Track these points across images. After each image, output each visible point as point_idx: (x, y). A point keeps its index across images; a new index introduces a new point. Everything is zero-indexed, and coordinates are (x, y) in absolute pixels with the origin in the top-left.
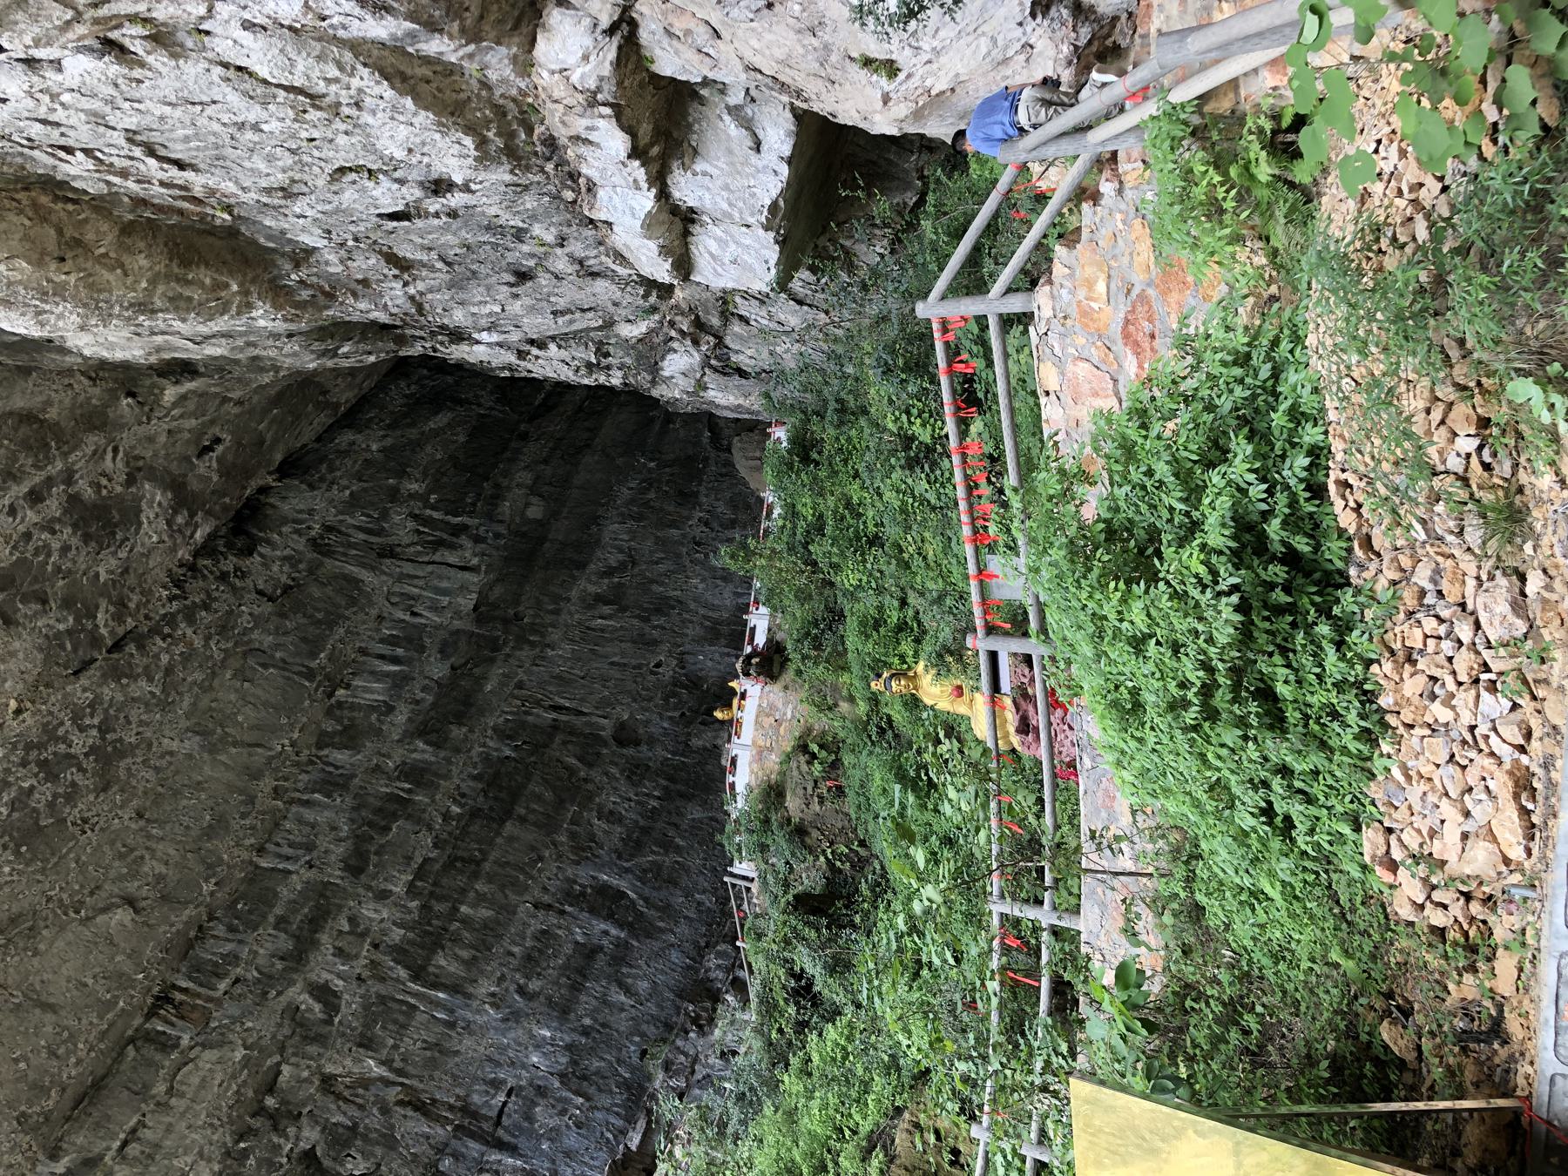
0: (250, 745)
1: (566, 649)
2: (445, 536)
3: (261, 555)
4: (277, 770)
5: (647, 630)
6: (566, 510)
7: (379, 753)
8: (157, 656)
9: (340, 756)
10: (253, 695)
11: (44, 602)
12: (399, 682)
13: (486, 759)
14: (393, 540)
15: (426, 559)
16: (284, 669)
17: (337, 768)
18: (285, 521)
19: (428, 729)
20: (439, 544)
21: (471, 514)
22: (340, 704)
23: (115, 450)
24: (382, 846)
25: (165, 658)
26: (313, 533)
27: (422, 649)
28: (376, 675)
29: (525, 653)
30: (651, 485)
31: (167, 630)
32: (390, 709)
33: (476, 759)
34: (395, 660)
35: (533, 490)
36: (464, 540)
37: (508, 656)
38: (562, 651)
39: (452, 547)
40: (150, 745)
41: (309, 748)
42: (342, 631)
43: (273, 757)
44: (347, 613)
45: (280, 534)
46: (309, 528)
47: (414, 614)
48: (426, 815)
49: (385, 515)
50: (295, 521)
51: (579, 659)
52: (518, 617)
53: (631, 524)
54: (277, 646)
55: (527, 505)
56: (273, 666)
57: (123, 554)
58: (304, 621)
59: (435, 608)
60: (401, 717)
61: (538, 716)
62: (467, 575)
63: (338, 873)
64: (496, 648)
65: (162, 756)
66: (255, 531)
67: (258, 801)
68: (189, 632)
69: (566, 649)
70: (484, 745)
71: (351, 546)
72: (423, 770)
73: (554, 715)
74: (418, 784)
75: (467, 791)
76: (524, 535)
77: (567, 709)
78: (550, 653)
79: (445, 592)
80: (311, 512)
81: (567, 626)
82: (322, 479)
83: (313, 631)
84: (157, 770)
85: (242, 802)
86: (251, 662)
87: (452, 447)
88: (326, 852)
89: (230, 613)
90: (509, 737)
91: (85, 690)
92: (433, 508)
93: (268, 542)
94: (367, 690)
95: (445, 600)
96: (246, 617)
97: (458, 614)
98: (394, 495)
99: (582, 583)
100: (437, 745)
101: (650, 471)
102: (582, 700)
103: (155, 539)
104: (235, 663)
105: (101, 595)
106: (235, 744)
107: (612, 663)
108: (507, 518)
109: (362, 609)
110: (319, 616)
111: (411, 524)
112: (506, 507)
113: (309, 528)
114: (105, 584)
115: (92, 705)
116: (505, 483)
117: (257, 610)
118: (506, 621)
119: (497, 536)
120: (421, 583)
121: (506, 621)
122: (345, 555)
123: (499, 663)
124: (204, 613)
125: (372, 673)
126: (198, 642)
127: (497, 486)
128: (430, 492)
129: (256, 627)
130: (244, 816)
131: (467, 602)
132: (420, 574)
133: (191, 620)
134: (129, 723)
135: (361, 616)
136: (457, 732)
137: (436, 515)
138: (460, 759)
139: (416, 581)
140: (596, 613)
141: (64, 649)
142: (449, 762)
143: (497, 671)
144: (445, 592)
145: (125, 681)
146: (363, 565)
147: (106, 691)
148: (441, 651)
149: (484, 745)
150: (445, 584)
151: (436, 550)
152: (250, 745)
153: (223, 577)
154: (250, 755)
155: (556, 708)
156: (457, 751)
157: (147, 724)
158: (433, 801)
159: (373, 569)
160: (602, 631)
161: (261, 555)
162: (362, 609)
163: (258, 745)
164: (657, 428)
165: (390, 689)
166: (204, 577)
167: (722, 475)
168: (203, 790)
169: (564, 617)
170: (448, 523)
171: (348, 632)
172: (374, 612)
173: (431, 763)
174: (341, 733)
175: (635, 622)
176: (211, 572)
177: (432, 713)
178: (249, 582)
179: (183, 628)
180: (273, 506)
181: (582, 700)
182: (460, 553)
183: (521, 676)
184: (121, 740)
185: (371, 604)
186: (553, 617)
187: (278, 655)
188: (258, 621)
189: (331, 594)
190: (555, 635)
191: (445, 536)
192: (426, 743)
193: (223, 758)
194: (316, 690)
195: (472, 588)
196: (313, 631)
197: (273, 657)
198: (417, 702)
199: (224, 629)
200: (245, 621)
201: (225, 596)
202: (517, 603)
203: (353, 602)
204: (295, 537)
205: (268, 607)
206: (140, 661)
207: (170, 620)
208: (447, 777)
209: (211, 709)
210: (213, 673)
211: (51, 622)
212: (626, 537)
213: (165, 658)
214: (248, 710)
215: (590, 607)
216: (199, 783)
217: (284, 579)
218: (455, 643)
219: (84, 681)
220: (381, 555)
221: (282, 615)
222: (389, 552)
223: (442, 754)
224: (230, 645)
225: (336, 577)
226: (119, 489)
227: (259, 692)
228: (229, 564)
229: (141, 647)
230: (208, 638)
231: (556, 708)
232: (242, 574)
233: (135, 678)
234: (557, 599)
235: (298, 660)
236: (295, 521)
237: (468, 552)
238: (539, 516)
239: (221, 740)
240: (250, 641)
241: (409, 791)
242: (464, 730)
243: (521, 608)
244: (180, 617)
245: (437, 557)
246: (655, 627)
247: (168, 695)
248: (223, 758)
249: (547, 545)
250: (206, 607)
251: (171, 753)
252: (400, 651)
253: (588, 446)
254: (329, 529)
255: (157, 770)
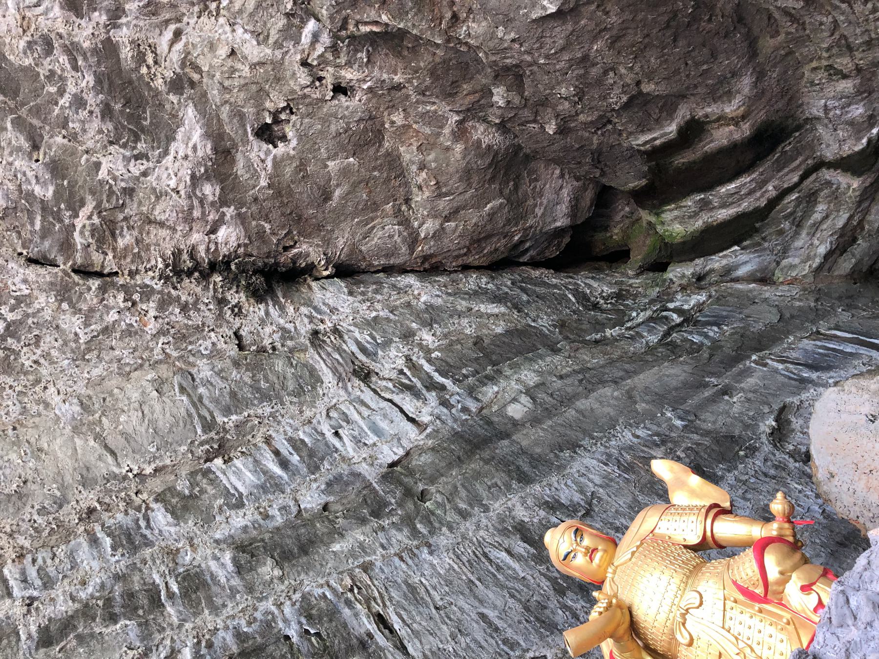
0: (106, 447)
1: (444, 562)
2: (419, 385)
3: (267, 313)
4: (108, 492)
5: (553, 604)
6: (550, 423)
7: (191, 540)
8: (108, 308)
9: (161, 517)
10: (151, 407)
11: (36, 147)
12: (271, 485)
13: (268, 625)
14: (373, 366)
15: (388, 396)
16: (194, 404)
17: (148, 526)
18: (309, 303)
19: (247, 551)
20: (410, 388)
21: (456, 381)
22: (207, 473)
23: (178, 34)
24: (92, 635)
25: (113, 316)
26: (321, 327)
27: (314, 469)
28: (258, 467)
29: (400, 537)
30: (663, 442)
31: (136, 297)
32: (240, 505)
33: (258, 615)
34: (284, 464)
35: (529, 392)
36: (432, 397)
37: (383, 528)
38: (438, 562)
39: (417, 395)
40: (38, 381)
41: (150, 494)
42: (268, 410)
43: (115, 476)
44: (287, 399)
45: (296, 310)
46: (322, 321)
47: (336, 434)
48: (158, 637)
49: (387, 344)
50: (315, 308)
51: (449, 583)
52: (423, 496)
53: (613, 470)
54: (208, 383)
55: (515, 400)
56: (189, 395)
57: (136, 169)
58: (248, 380)
59: (358, 441)
60: (239, 520)
61: (356, 615)
62: (409, 426)
63: (33, 628)
64: (377, 514)
65: (38, 402)
66: (280, 294)
67: (66, 508)
68: (152, 313)
69: (444, 562)
70: (279, 606)
71: (339, 350)
72: (205, 584)
73: (372, 627)
74: (186, 594)
75: (217, 642)
76: (489, 423)
77: (392, 631)
78: (425, 554)
79: (377, 432)
80: (333, 310)
81: (464, 537)
82: (363, 294)
83: (247, 393)
84: (24, 410)
85: (53, 496)
86: (176, 380)
87: (485, 331)
88: (52, 600)
89: (199, 329)
90: (309, 617)
91: (25, 281)
92: (429, 361)
93: (282, 308)
94: (238, 473)
95: (372, 439)
96: (208, 343)
97: (372, 460)
98: (407, 336)
99: (514, 500)
100: (239, 569)
101: (672, 427)
102: (416, 634)
103: (173, 183)
104: (164, 371)
105: (93, 193)
106: (97, 437)
107: (483, 616)
108: (485, 399)
109: (301, 404)
110: (263, 385)
111: (400, 363)
112: (490, 390)
113: (322, 321)
114: (101, 182)
115: (19, 300)
116: (508, 372)
117: (221, 345)
118: (408, 493)
119: (465, 410)
120: (366, 412)
121: (408, 493)
122: (329, 355)
123: (367, 529)
124: (177, 310)
125: (256, 462)
126: (152, 327)
127: (499, 372)
128: (437, 349)
129: (210, 357)
130: (42, 511)
131: (389, 454)
132: (373, 405)
133: (163, 305)
134: (37, 345)
135: (294, 409)
136: (268, 569)
137: (427, 367)
138: (244, 600)
139: (363, 409)
140: (506, 543)
141: (32, 224)
142: (234, 591)
143: (358, 535)
144: (377, 432)
145: (65, 306)
146: (335, 371)
147: (42, 299)
148: (329, 484)
149: (279, 606)
150: (384, 425)
151: (402, 391)
152: (106, 447)
153: (222, 302)
154: (100, 458)
155: (381, 621)
156: (250, 589)
157: (52, 362)
158: (180, 626)
159: (340, 379)
160: (499, 568)
161: (267, 313)
162: (301, 404)
163: (113, 453)
164: (706, 394)
165: (257, 487)
166: (206, 288)
167: (766, 475)
168: (38, 458)
169: (468, 526)
170: (431, 378)
171: (272, 415)
172: (308, 413)
173: (217, 583)
174: (184, 498)
175: (545, 584)
176: (215, 290)
177: (267, 536)
178: (237, 322)
179: (151, 307)
180: (310, 288)
181: (416, 634)
182: (419, 404)
183: (376, 558)
184: (17, 354)
185: (312, 405)
186: (457, 518)
187: (201, 390)
188: (215, 353)
189: (289, 375)
190: (444, 539)
191: (419, 385)
192: (235, 560)
193: (79, 442)
194: (202, 444)
195: (405, 443)
196: (247, 393)
197: (195, 388)
198: (266, 516)
199: (182, 338)
200: (204, 346)
201: (208, 313)
202: (432, 480)
203: (299, 392)
204: (306, 320)
205: (232, 350)
206: (91, 298)
207: (147, 292)
208: (215, 610)
209: (111, 394)
210: (141, 365)
211: (30, 174)
212: (598, 480)
213: (113, 316)
214: (135, 416)
215: (504, 532)
216: (40, 450)
217: (267, 342)
218: (347, 484)
219: (32, 273)
220: (355, 373)
221: (236, 364)
222: (365, 375)
223: (236, 582)
224: (175, 354)
225: (305, 365)
226: (159, 83)
227: (158, 407)
228: (235, 297)
229: (103, 289)
230: (161, 332)
231: (381, 621)
232: (237, 310)
233: (77, 311)
234: (475, 500)
235: (211, 406)
236: (315, 308)
237: (427, 410)
238: (518, 416)
239: (91, 424)
240: (194, 365)
241: (171, 595)
242: (277, 572)
243: (433, 489)
244: (157, 297)
245: (397, 399)
246: (565, 607)
247: (89, 350)
248: (79, 442)
249: (506, 442)
250: (184, 308)
251: (47, 405)
252: (295, 458)
253: (616, 383)
254: (335, 330)
255: (24, 410)
